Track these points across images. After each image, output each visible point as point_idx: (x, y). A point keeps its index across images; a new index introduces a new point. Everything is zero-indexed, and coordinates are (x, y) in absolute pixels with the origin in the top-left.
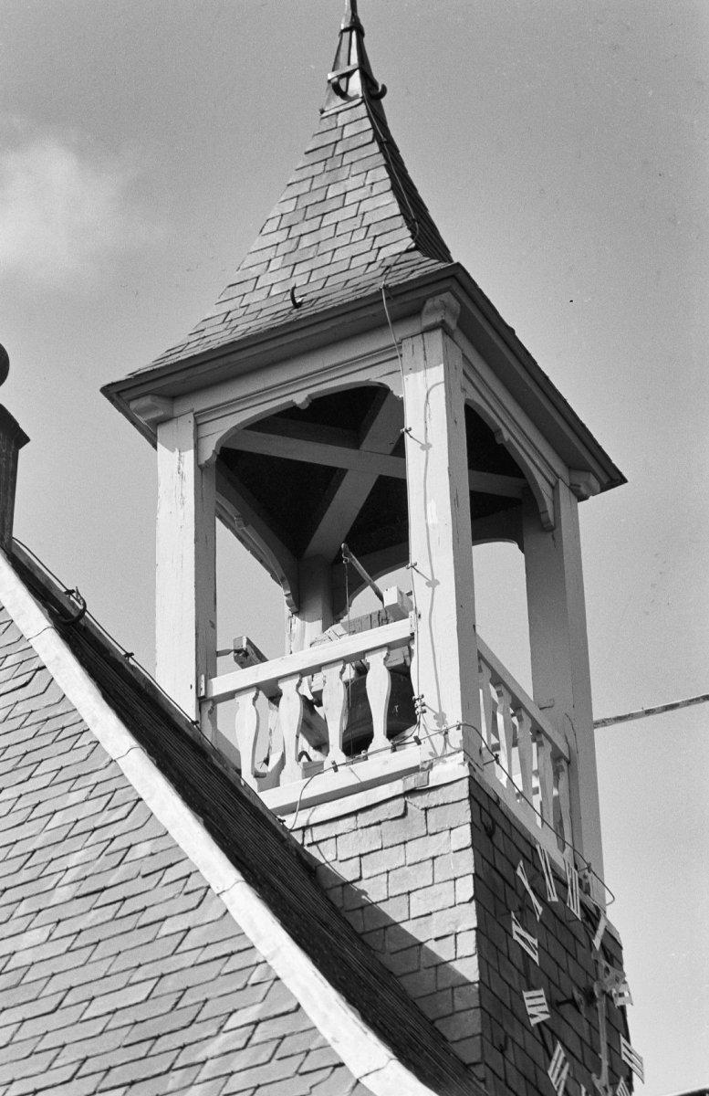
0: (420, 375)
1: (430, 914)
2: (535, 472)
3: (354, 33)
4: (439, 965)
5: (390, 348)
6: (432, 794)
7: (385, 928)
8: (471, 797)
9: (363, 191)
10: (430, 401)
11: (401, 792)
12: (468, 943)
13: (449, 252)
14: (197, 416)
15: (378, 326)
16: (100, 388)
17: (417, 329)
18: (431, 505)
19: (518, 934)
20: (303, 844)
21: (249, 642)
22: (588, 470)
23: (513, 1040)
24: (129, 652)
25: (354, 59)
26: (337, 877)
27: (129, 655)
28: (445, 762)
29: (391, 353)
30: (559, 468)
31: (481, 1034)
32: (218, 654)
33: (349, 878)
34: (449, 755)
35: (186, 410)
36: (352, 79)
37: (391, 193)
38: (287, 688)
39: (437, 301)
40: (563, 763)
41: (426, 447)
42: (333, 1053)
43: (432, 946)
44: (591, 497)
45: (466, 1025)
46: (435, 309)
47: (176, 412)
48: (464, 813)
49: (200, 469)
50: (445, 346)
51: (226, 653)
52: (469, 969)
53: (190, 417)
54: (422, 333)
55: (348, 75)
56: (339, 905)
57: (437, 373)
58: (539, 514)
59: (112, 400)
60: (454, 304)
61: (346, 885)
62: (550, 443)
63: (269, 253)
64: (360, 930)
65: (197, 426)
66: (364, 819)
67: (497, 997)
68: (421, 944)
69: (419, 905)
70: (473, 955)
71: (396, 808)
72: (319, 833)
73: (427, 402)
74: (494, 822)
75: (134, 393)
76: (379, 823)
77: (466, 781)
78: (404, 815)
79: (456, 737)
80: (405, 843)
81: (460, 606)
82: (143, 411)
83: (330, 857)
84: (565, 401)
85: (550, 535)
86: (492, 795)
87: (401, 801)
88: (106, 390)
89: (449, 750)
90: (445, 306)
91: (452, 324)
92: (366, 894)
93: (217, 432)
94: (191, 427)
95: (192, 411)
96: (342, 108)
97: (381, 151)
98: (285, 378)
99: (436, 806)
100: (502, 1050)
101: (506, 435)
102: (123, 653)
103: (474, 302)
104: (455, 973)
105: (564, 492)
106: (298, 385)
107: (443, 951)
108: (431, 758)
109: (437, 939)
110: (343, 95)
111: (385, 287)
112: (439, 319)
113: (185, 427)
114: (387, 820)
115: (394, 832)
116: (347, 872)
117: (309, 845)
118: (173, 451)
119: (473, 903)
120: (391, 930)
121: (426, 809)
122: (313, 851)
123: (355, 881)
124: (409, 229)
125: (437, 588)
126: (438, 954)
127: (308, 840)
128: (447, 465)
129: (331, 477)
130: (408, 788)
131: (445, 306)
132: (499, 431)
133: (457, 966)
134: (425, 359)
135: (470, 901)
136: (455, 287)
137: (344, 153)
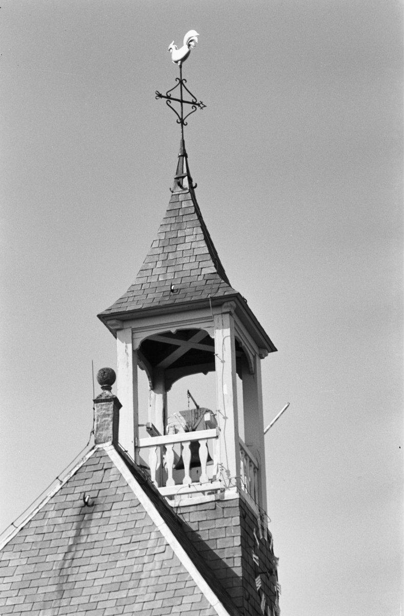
0: (221, 331)
1: (224, 548)
2: (249, 353)
3: (184, 158)
4: (228, 569)
5: (210, 317)
6: (225, 503)
7: (208, 551)
8: (240, 506)
9: (192, 237)
10: (225, 343)
11: (214, 499)
12: (238, 562)
13: (224, 271)
14: (133, 330)
15: (207, 307)
16: (97, 315)
17: (220, 312)
18: (225, 386)
19: (255, 558)
20: (177, 513)
21: (153, 425)
22: (265, 348)
23: (252, 596)
24: (126, 450)
25: (185, 171)
26: (190, 528)
27: (126, 451)
28: (229, 490)
29: (210, 319)
30: (257, 350)
31: (243, 597)
32: (139, 425)
33: (194, 529)
34: (231, 487)
35: (128, 326)
36: (184, 179)
37: (204, 242)
38: (169, 447)
39: (229, 304)
40: (256, 470)
41: (223, 362)
42: (109, 459)
43: (225, 560)
44: (265, 358)
45: (238, 592)
46: (228, 306)
47: (125, 327)
48: (237, 512)
49: (134, 351)
50: (230, 319)
51: (143, 425)
52: (239, 572)
53: (130, 330)
54: (222, 314)
55: (183, 177)
56: (190, 539)
57: (227, 332)
58: (249, 369)
59: (102, 321)
60: (235, 305)
61: (193, 532)
62: (256, 344)
63: (156, 258)
64: (199, 550)
65: (133, 333)
66: (199, 508)
67: (247, 581)
68: (221, 559)
69: (220, 544)
70: (240, 567)
71: (212, 506)
72: (182, 511)
73: (223, 343)
74: (246, 513)
75: (109, 318)
76: (205, 510)
77: (238, 500)
78: (215, 509)
79: (234, 481)
80: (215, 519)
81: (235, 428)
82: (113, 325)
83: (187, 520)
84: (263, 330)
85: (252, 376)
86: (243, 500)
87: (214, 503)
88: (99, 316)
89: (231, 485)
90: (231, 306)
91: (233, 311)
92: (200, 536)
93: (142, 336)
94: (131, 333)
95: (131, 327)
96: (181, 192)
97: (198, 219)
98: (170, 321)
99: (227, 507)
100: (248, 600)
101: (243, 344)
102: (124, 450)
103: (249, 315)
104: (233, 572)
105: (257, 358)
106: (173, 324)
107: (223, 556)
108: (224, 487)
109: (227, 558)
110: (181, 186)
111: (211, 298)
112: (229, 311)
113: (128, 333)
114: (208, 509)
115: (211, 515)
116: (194, 527)
117: (179, 514)
118: (123, 343)
119: (240, 547)
120: (210, 551)
121: (223, 508)
122: (180, 516)
123: (197, 531)
124: (213, 262)
125: (227, 420)
126: (227, 564)
127: (179, 512)
128: (231, 371)
129: (177, 347)
130: (217, 499)
131: (231, 306)
132: (241, 343)
133: (234, 569)
134: (223, 325)
135: (239, 546)
136: (237, 300)
137: (183, 215)
